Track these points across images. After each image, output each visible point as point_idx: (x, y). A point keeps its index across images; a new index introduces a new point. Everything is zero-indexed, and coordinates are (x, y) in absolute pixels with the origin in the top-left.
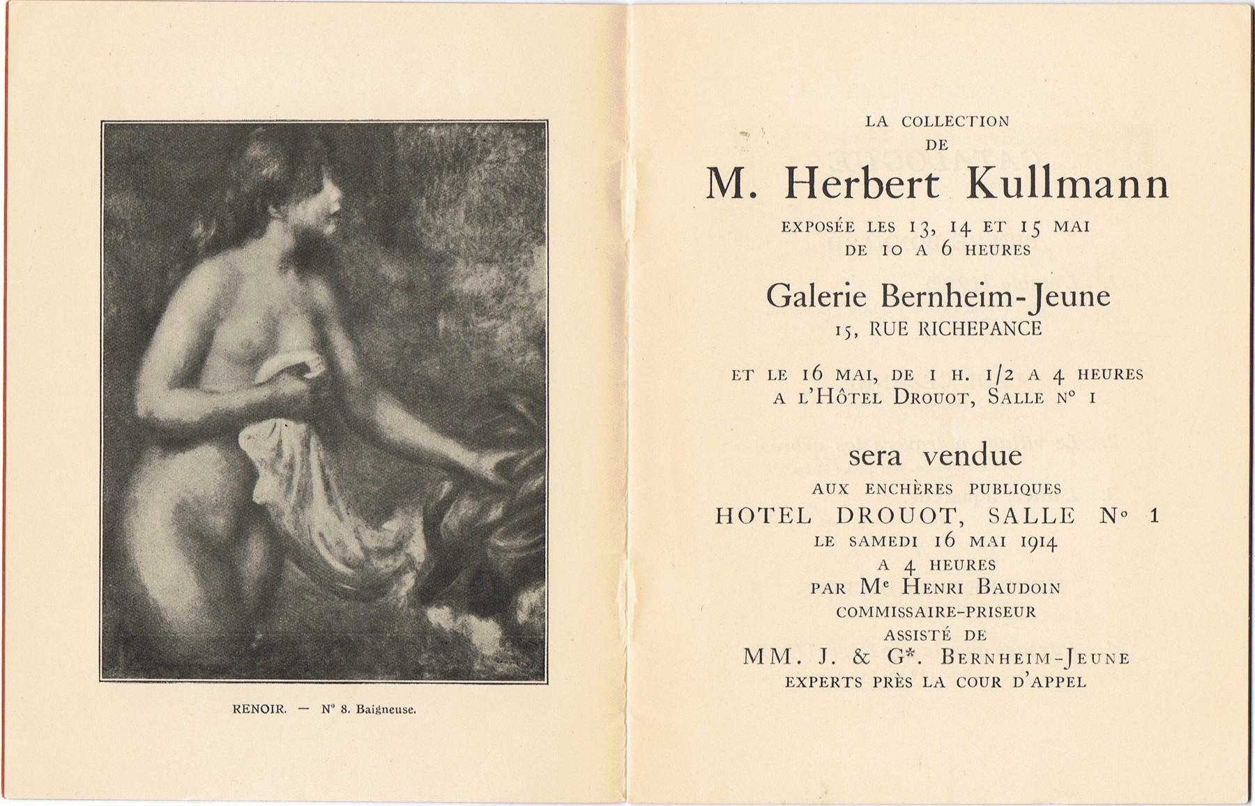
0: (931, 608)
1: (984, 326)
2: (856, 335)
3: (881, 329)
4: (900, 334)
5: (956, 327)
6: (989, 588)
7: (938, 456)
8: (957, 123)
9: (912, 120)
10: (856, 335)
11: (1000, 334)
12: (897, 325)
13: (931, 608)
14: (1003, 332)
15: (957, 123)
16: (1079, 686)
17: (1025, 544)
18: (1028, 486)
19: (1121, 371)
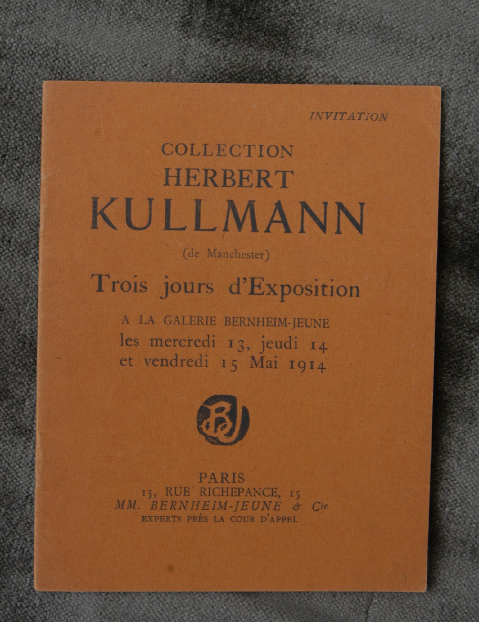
0: (326, 204)
1: (241, 490)
2: (155, 495)
3: (173, 492)
4: (168, 227)
5: (175, 179)
6: (233, 180)
7: (151, 361)
8: (177, 151)
9: (202, 342)
10: (155, 495)
11: (251, 495)
12: (183, 490)
13: (326, 204)
14: (253, 494)
15: (177, 151)
16: (183, 324)
17: (310, 364)
18: (185, 146)
19: (215, 174)
